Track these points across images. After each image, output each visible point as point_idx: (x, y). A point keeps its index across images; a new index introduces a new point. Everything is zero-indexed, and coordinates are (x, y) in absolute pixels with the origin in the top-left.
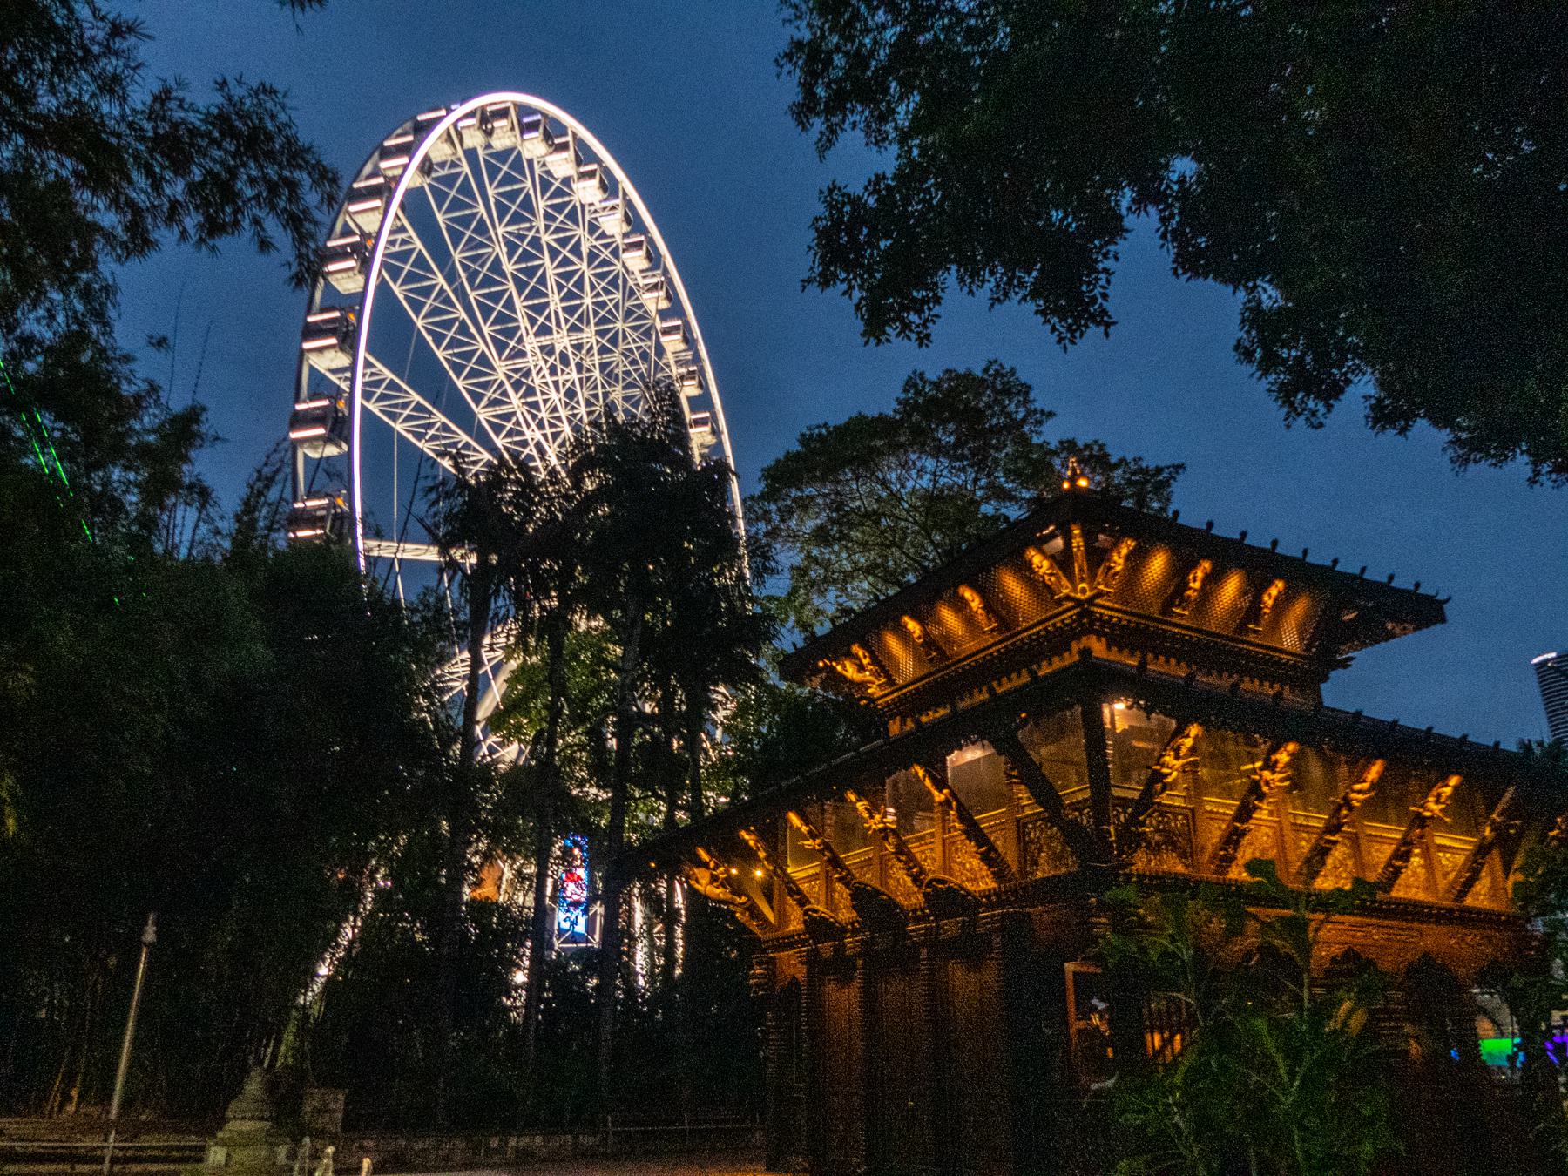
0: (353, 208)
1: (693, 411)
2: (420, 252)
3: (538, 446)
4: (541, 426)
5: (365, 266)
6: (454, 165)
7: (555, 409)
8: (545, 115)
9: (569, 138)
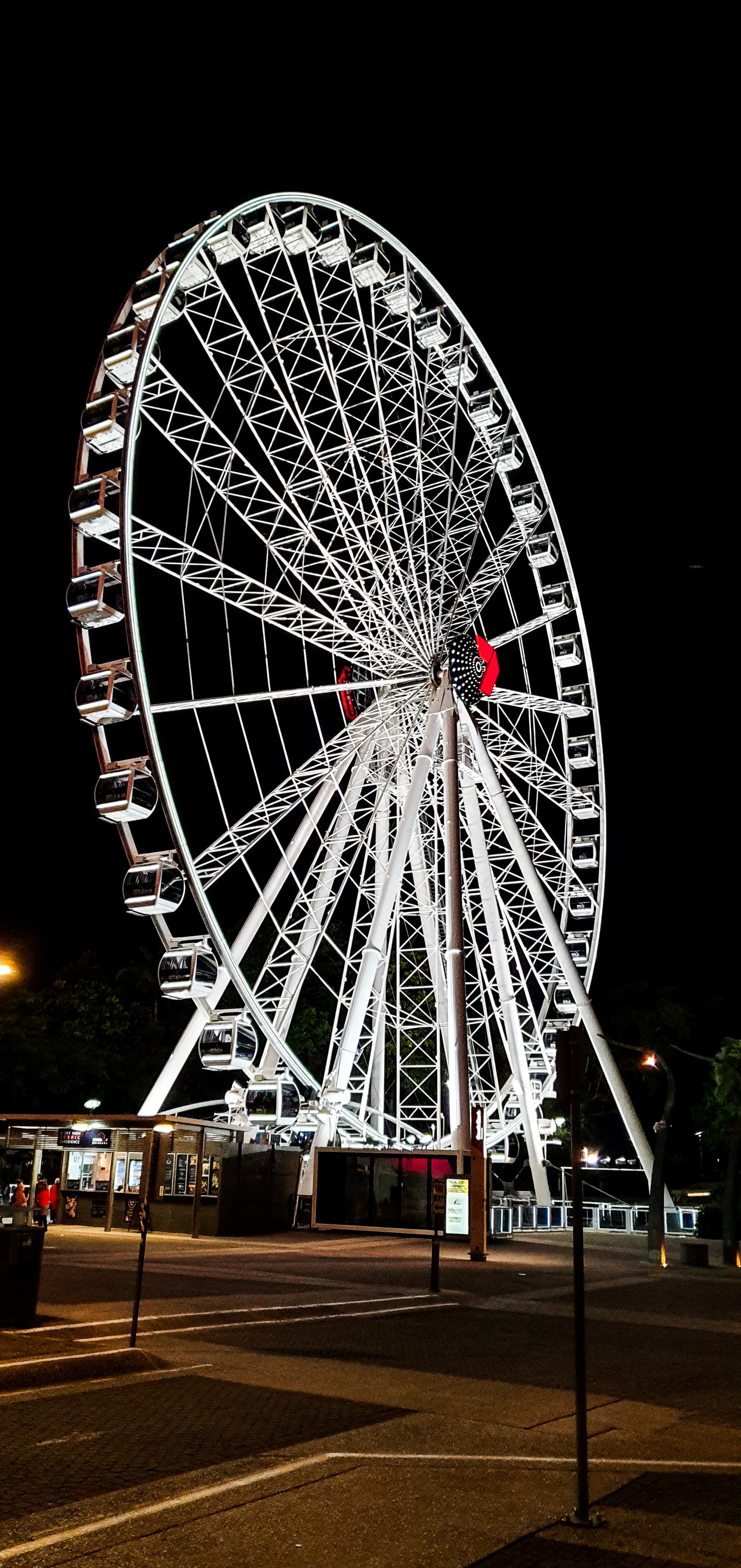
0: (107, 361)
1: (513, 485)
2: (181, 393)
3: (354, 594)
4: (354, 576)
5: (124, 421)
6: (211, 290)
7: (365, 557)
8: (306, 204)
9: (340, 222)
